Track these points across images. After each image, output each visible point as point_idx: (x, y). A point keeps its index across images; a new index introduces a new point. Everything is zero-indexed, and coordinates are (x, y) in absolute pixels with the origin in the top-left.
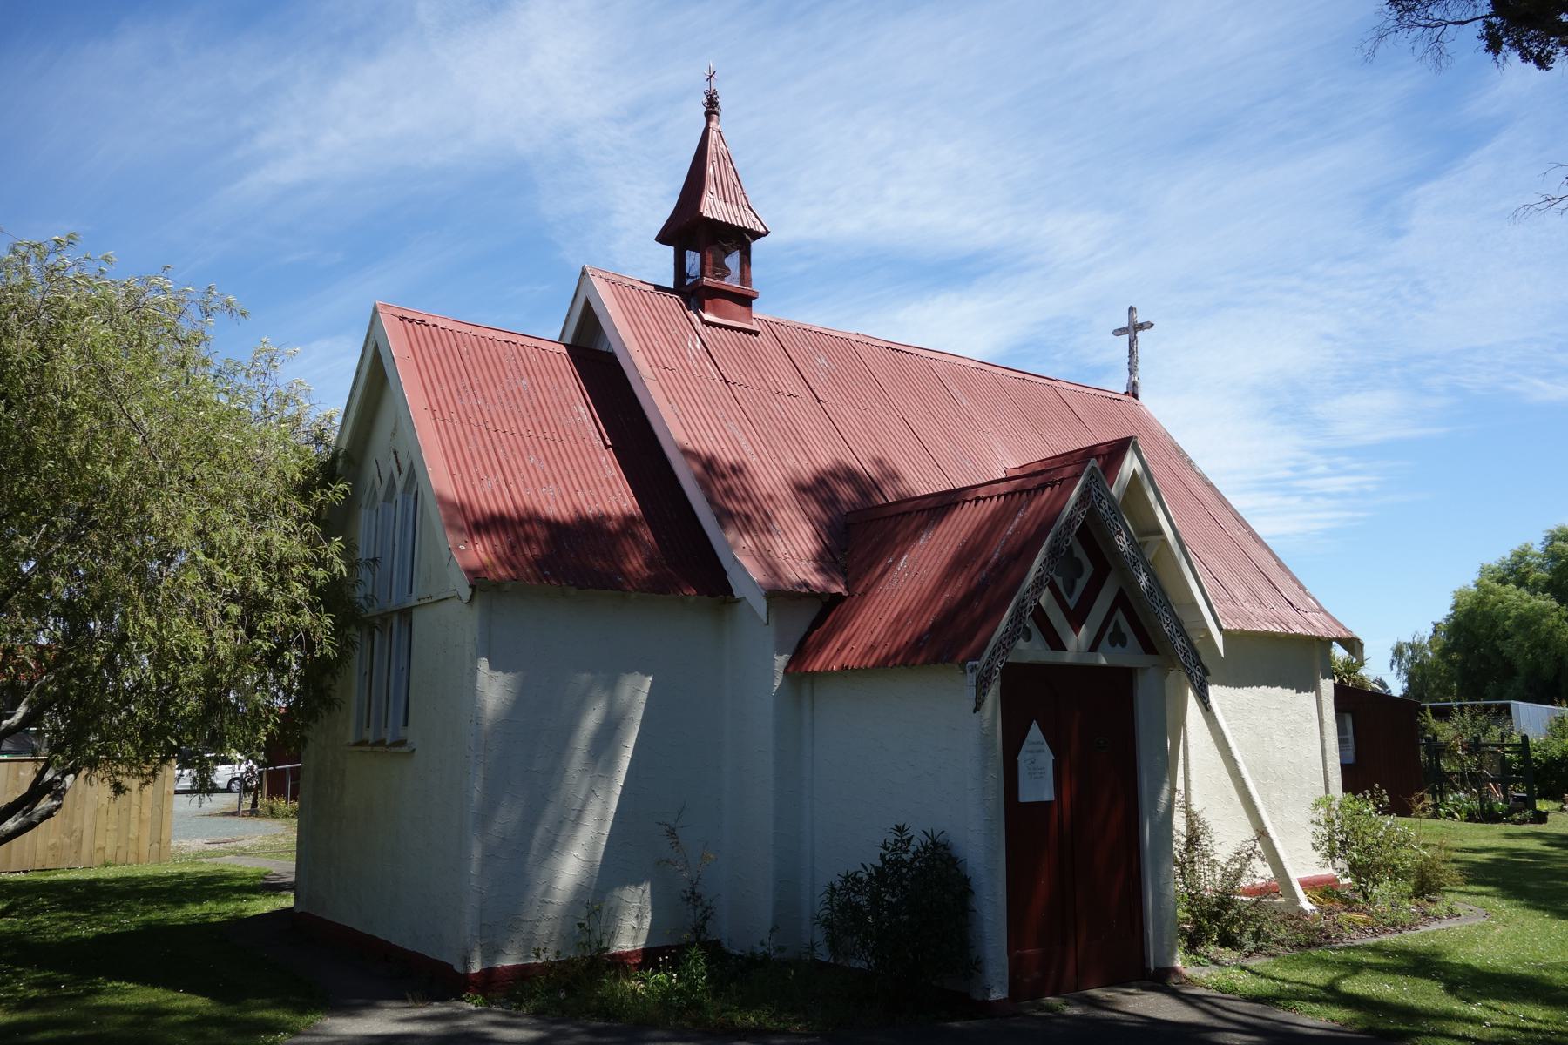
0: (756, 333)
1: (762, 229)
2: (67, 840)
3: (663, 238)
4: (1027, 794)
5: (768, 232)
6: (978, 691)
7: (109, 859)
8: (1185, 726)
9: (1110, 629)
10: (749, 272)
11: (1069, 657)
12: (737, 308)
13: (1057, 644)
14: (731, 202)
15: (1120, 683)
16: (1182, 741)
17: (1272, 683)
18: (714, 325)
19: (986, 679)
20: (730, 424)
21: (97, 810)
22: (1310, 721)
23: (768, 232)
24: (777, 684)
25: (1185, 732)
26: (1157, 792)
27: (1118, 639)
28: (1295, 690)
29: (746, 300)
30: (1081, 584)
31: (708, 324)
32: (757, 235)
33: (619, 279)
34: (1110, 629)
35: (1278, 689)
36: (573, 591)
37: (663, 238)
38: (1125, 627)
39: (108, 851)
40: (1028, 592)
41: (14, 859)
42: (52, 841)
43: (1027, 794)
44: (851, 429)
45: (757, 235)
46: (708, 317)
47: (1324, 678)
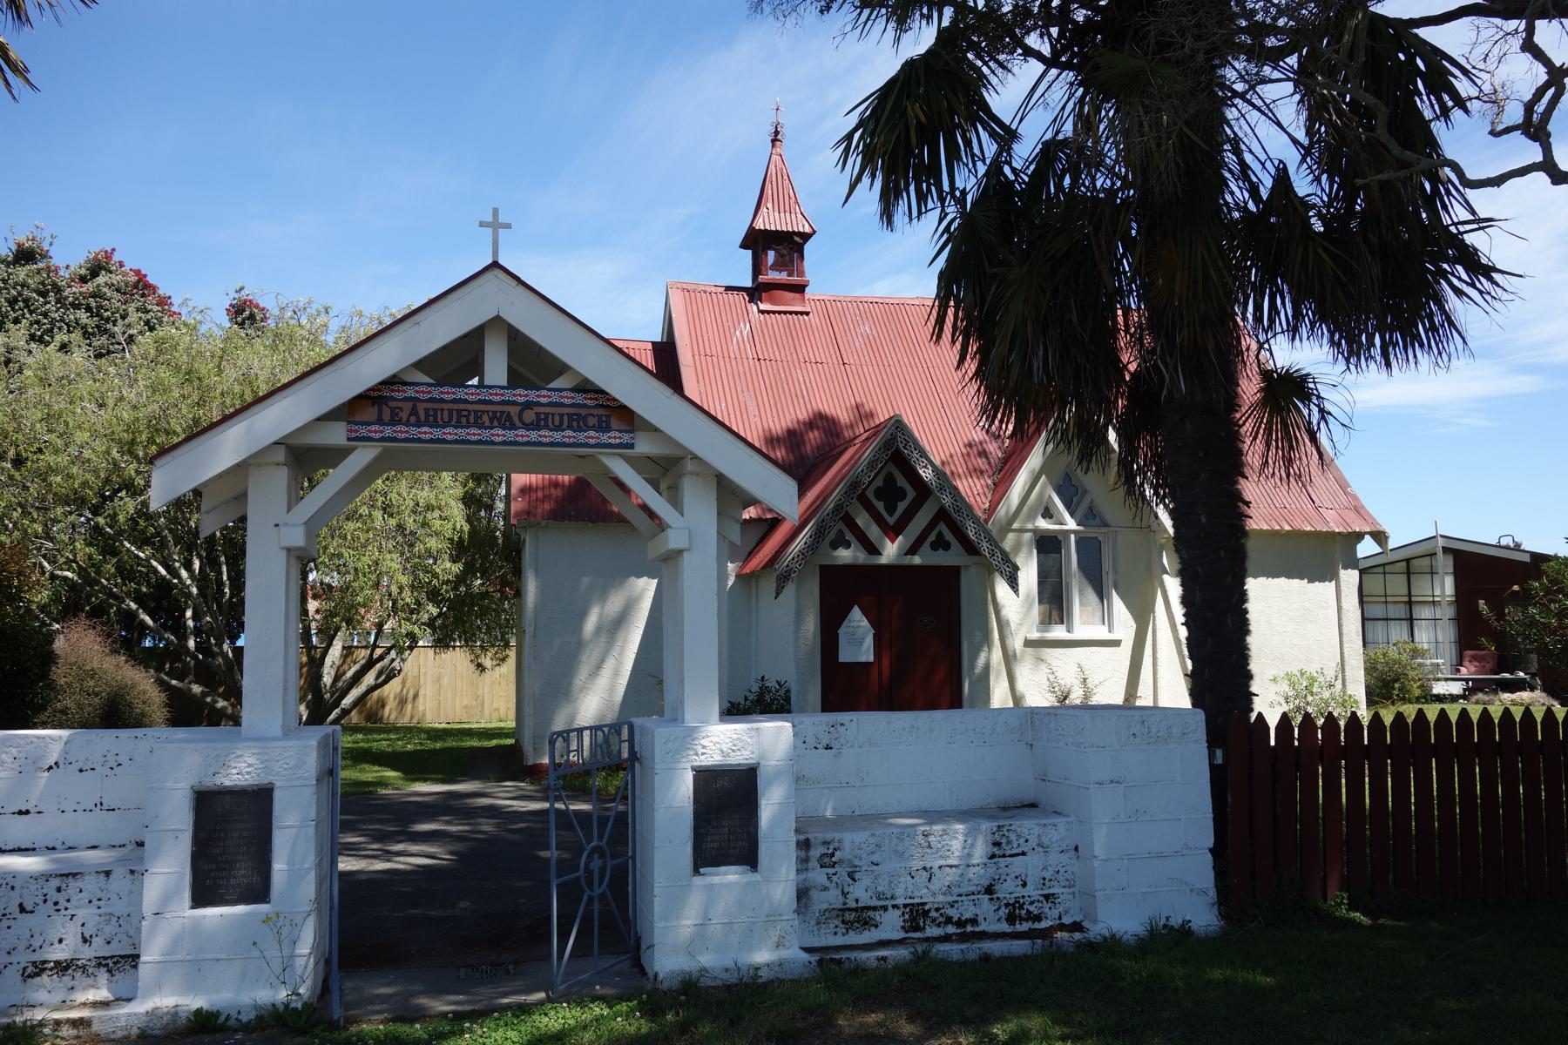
0: (807, 314)
1: (807, 230)
2: (475, 703)
3: (744, 246)
4: (846, 655)
5: (814, 232)
6: (778, 585)
7: (502, 716)
8: (1154, 612)
9: (932, 537)
10: (803, 266)
11: (883, 560)
12: (789, 295)
13: (874, 550)
14: (785, 211)
15: (951, 576)
16: (1151, 625)
17: (1290, 575)
18: (768, 312)
19: (785, 577)
20: (746, 394)
21: (493, 682)
22: (1326, 608)
23: (814, 232)
24: (730, 583)
25: (1154, 617)
26: (974, 657)
27: (940, 544)
28: (1306, 581)
29: (800, 289)
30: (902, 506)
31: (763, 312)
32: (806, 237)
33: (694, 287)
34: (932, 537)
35: (1283, 580)
36: (590, 525)
37: (744, 246)
38: (948, 536)
39: (501, 711)
40: (828, 515)
41: (442, 715)
42: (465, 703)
43: (846, 655)
44: (865, 387)
45: (806, 237)
46: (763, 307)
47: (1345, 568)
